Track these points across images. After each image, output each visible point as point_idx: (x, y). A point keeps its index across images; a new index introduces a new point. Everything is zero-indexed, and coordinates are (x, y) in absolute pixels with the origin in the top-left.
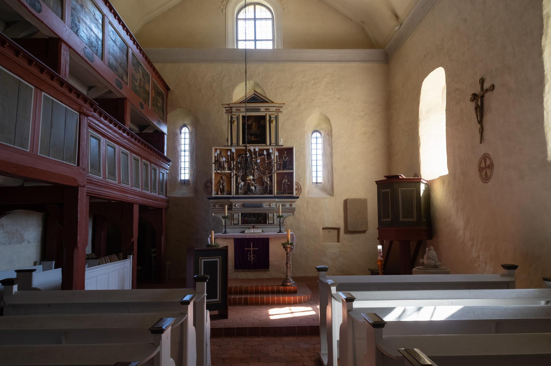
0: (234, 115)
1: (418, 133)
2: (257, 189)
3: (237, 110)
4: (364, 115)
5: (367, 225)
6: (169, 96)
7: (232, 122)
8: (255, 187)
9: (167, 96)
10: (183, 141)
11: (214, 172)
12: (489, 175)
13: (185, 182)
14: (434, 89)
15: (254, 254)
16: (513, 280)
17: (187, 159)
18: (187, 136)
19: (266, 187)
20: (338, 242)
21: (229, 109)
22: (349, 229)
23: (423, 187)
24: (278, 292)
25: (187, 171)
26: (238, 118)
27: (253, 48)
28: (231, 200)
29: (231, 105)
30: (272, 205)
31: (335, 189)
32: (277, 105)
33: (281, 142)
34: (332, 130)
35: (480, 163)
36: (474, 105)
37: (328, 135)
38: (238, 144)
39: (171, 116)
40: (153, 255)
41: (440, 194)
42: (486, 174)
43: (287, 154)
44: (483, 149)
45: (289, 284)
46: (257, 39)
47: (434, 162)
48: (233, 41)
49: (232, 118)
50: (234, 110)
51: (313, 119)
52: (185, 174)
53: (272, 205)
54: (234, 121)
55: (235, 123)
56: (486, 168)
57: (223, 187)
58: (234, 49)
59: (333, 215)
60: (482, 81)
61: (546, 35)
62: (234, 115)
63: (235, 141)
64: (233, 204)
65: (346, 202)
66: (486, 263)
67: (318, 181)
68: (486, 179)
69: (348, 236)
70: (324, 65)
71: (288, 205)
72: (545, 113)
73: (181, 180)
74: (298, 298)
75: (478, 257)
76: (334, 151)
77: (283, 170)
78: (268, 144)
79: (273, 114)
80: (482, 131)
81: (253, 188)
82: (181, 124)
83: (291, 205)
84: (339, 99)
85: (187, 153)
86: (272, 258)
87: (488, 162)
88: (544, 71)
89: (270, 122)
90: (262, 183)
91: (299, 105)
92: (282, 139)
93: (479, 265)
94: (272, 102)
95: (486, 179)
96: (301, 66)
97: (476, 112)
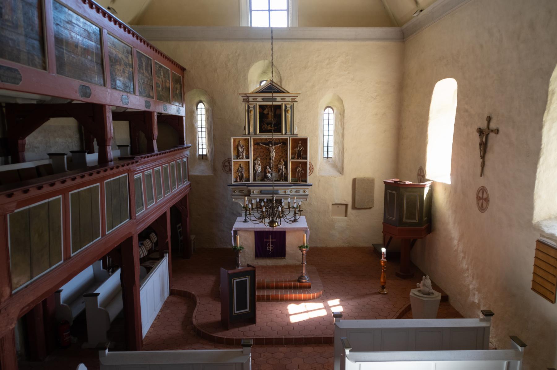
0: (251, 104)
1: (427, 131)
2: (274, 175)
3: (254, 99)
4: (377, 96)
5: (373, 203)
6: (186, 76)
7: (249, 112)
8: (271, 174)
9: (183, 77)
10: (199, 117)
11: (233, 161)
12: (484, 207)
13: (203, 157)
14: (445, 96)
15: (271, 244)
16: (488, 325)
17: (204, 134)
18: (204, 112)
19: (282, 174)
20: (346, 216)
21: (246, 99)
22: (356, 206)
23: (426, 190)
24: (295, 288)
25: (204, 147)
26: (255, 107)
27: (268, 26)
28: (250, 188)
29: (248, 95)
30: (288, 193)
31: (345, 169)
32: (293, 95)
33: (296, 132)
34: (344, 111)
35: (478, 192)
36: (481, 137)
37: (340, 114)
38: (255, 133)
39: (187, 96)
40: (179, 231)
41: (441, 199)
42: (482, 205)
43: (301, 145)
44: (482, 182)
45: (304, 281)
46: (271, 9)
47: (439, 167)
48: (247, 12)
49: (249, 107)
50: (251, 99)
51: (327, 98)
52: (203, 149)
53: (288, 193)
54: (251, 111)
55: (252, 112)
56: (483, 199)
57: (242, 174)
58: (249, 27)
59: (341, 191)
60: (489, 119)
61: (549, 111)
62: (251, 104)
63: (252, 130)
64: (252, 191)
65: (354, 180)
66: (473, 277)
67: (329, 156)
68: (482, 209)
69: (355, 211)
70: (339, 43)
71: (301, 192)
72: (536, 182)
73: (199, 155)
74: (312, 295)
75: (468, 269)
76: (345, 132)
77: (298, 159)
78: (284, 133)
79: (288, 104)
80: (483, 165)
81: (269, 175)
82: (197, 100)
83: (304, 192)
84: (353, 79)
85: (204, 129)
86: (288, 248)
87: (485, 196)
88: (541, 145)
89: (286, 111)
90: (279, 170)
91: (313, 86)
92: (296, 128)
93: (468, 276)
94: (288, 93)
95: (482, 209)
96: (317, 45)
97: (480, 148)
